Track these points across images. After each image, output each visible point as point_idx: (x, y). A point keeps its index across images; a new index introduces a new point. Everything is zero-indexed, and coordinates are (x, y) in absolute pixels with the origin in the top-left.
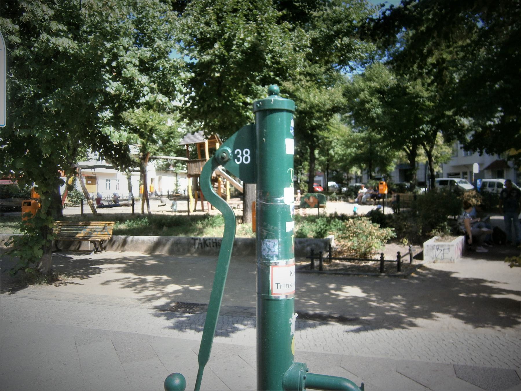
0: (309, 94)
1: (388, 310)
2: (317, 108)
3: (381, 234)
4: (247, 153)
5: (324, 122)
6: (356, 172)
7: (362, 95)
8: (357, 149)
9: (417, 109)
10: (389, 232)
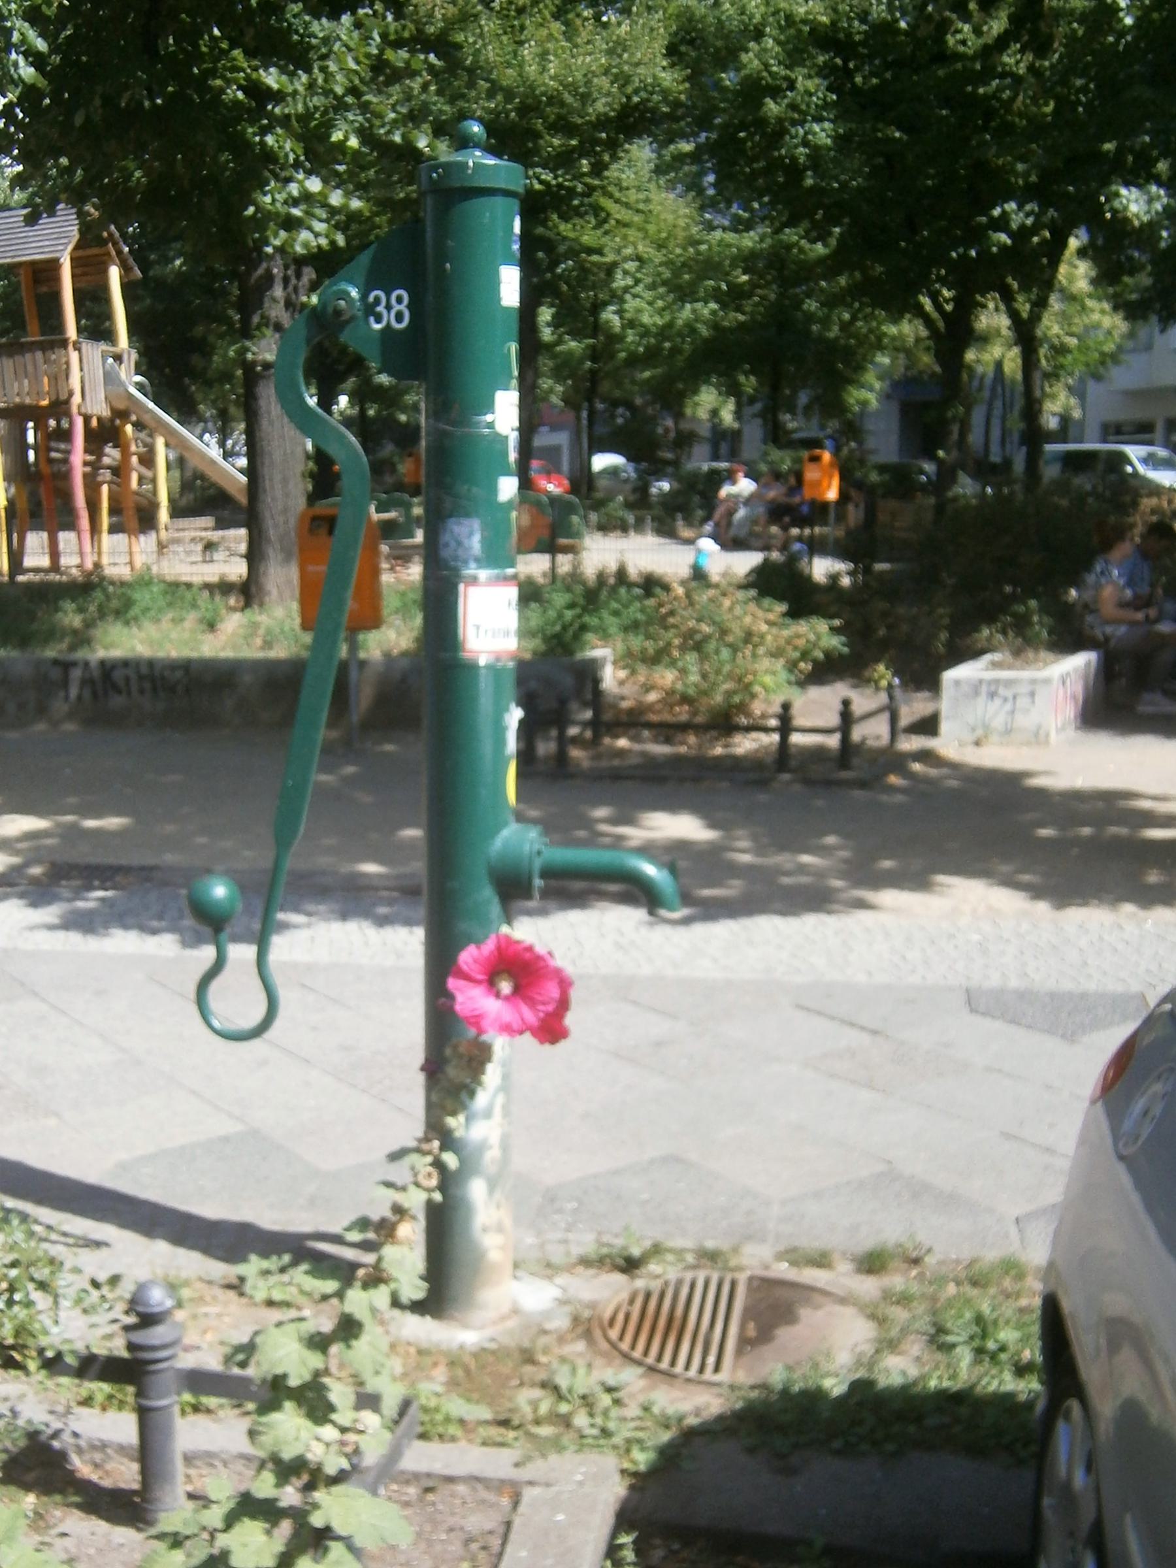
0: (520, 43)
1: (787, 873)
2: (552, 112)
3: (789, 642)
4: (399, 300)
5: (579, 176)
6: (715, 413)
7: (750, 59)
8: (724, 306)
9: (985, 129)
10: (820, 634)
